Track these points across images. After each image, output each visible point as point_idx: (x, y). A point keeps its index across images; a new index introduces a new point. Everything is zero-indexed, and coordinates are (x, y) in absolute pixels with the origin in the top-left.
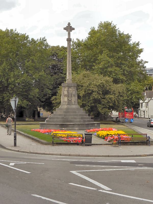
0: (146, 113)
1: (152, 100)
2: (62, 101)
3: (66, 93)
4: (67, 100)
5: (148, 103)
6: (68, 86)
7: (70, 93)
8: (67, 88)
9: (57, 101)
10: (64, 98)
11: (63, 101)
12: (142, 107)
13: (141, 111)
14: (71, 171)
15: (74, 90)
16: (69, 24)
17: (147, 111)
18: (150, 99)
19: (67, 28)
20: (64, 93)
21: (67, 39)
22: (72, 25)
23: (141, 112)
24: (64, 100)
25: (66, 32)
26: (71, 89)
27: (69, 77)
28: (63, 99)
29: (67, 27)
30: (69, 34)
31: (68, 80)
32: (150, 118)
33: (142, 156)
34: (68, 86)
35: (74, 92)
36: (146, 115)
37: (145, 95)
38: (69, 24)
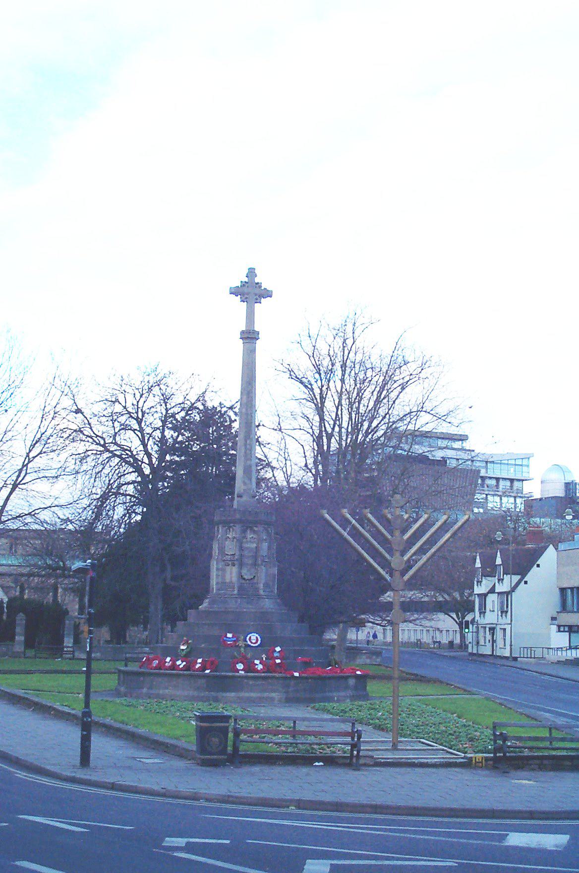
0: (499, 634)
1: (526, 583)
2: (217, 583)
3: (231, 548)
4: (235, 579)
5: (508, 593)
6: (240, 521)
7: (247, 548)
8: (238, 528)
9: (484, 587)
10: (223, 570)
11: (220, 580)
12: (483, 612)
13: (477, 628)
14: (18, 863)
15: (265, 540)
16: (251, 273)
17: (505, 630)
18: (516, 578)
19: (246, 290)
20: (222, 549)
21: (243, 332)
22: (238, 278)
23: (481, 630)
24: (224, 576)
25: (239, 307)
26: (254, 532)
27: (245, 483)
28: (220, 573)
29: (244, 284)
30: (250, 316)
31: (240, 496)
32: (515, 659)
33: (369, 810)
34: (240, 521)
35: (265, 545)
36: (500, 643)
37: (478, 564)
38: (251, 273)
